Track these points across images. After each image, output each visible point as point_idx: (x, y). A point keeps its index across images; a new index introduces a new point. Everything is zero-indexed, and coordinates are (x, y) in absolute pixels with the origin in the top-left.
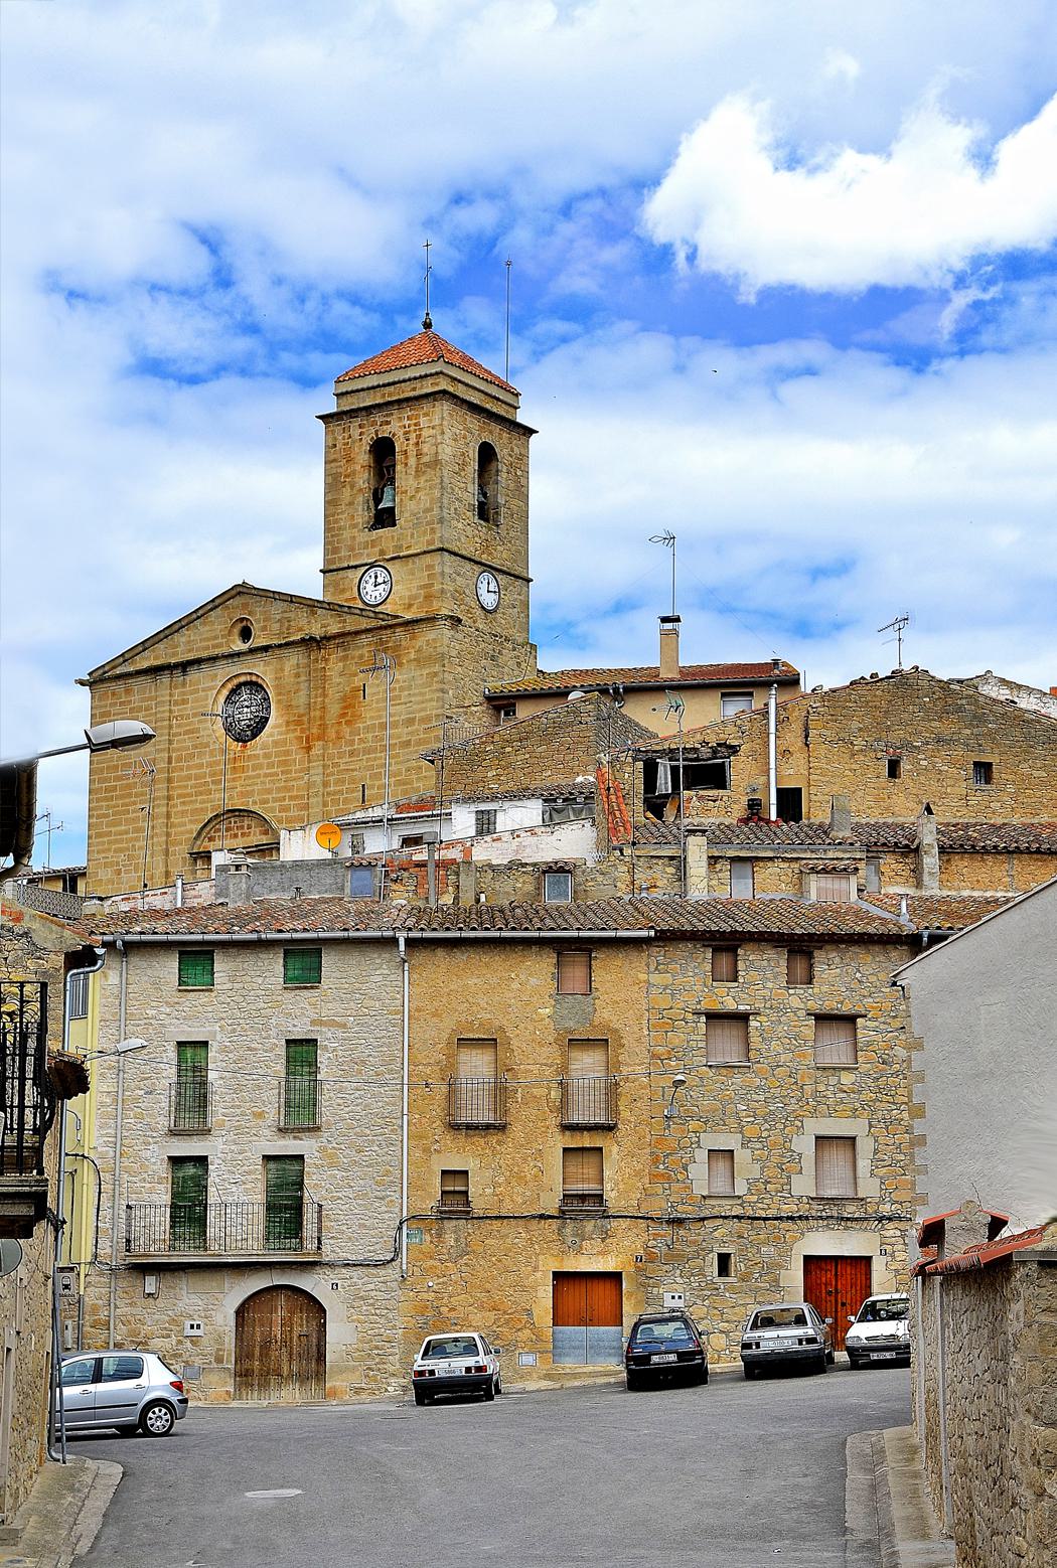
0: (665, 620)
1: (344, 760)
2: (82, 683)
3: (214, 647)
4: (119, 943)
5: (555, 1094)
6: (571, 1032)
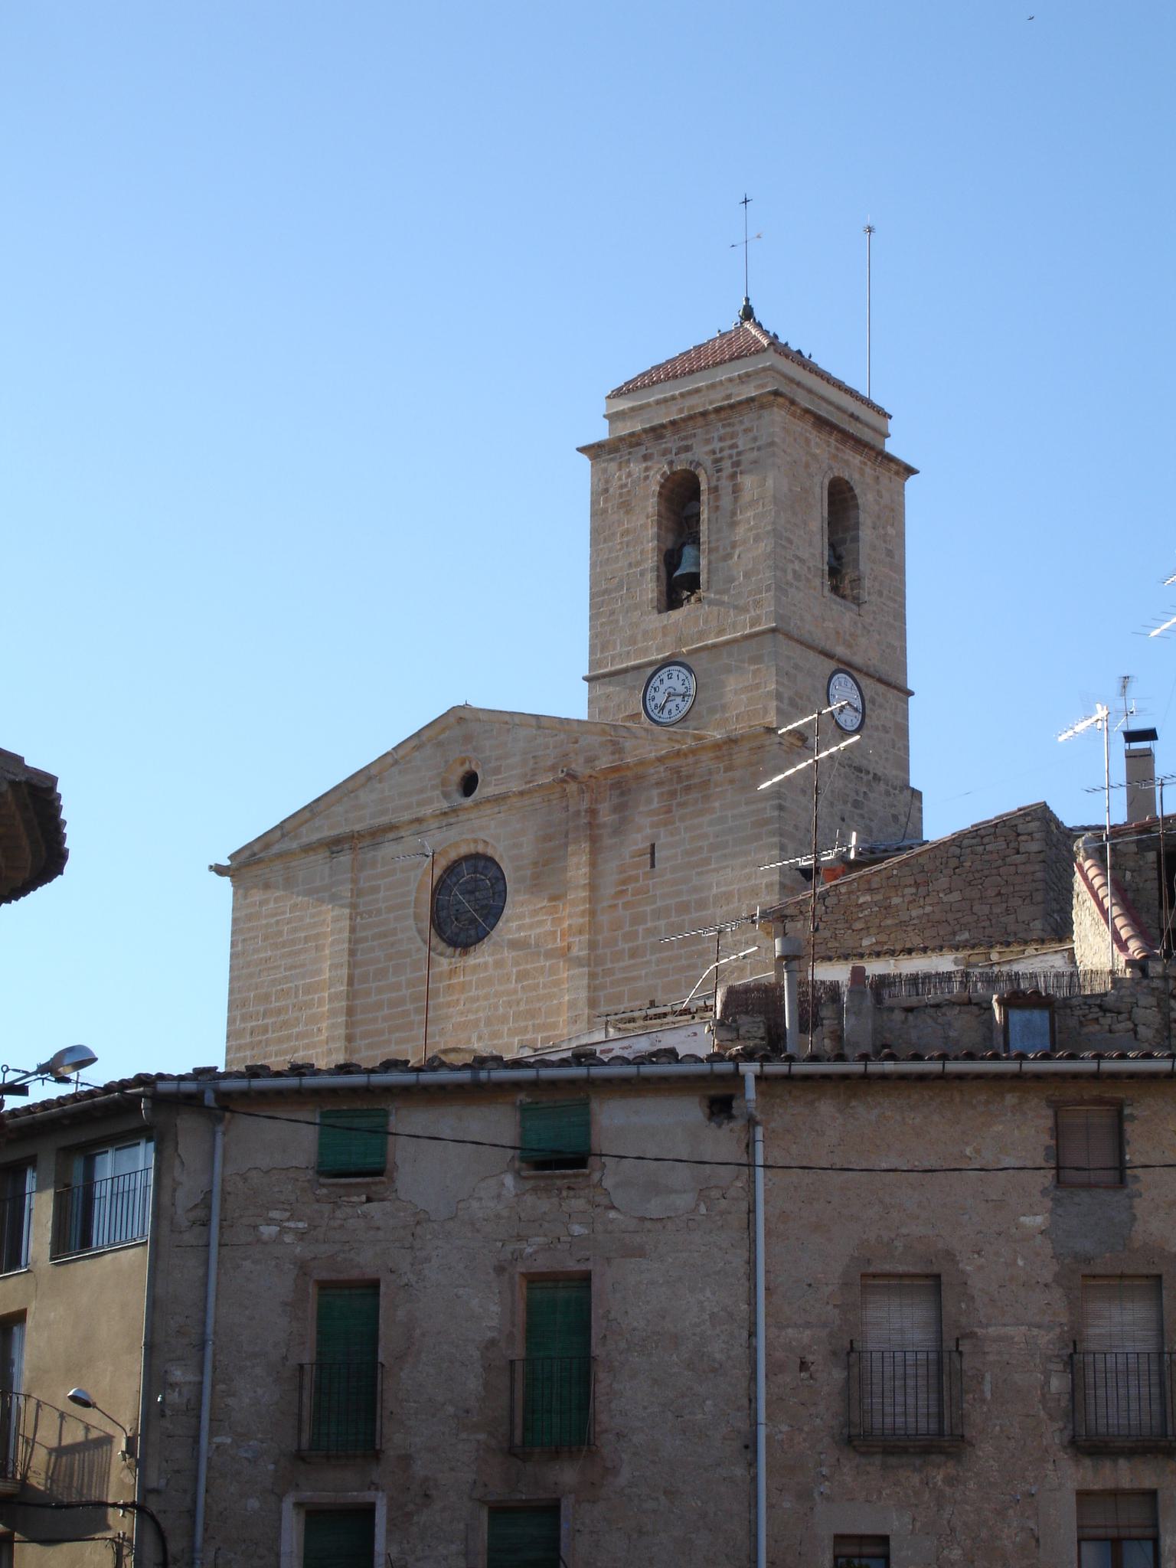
0: (1131, 736)
1: (621, 964)
2: (219, 870)
3: (420, 804)
4: (209, 1099)
5: (1058, 1384)
6: (1088, 1260)
